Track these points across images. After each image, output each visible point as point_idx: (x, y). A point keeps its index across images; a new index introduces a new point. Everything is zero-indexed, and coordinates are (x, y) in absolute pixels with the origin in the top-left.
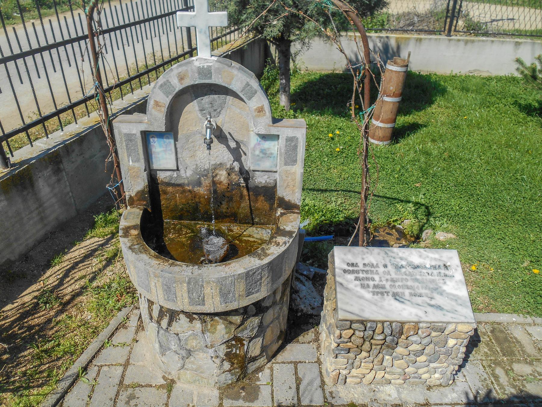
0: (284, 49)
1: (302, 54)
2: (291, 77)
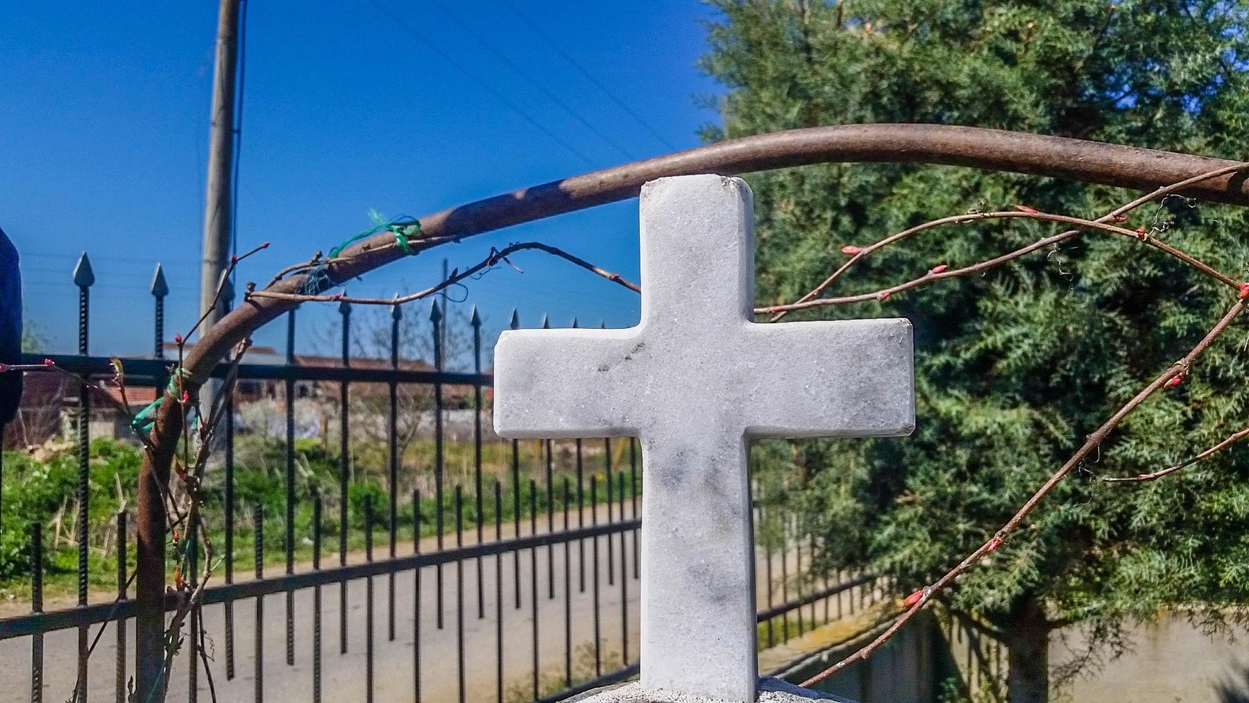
0: (1027, 653)
1: (1094, 670)
2: (1210, 392)
